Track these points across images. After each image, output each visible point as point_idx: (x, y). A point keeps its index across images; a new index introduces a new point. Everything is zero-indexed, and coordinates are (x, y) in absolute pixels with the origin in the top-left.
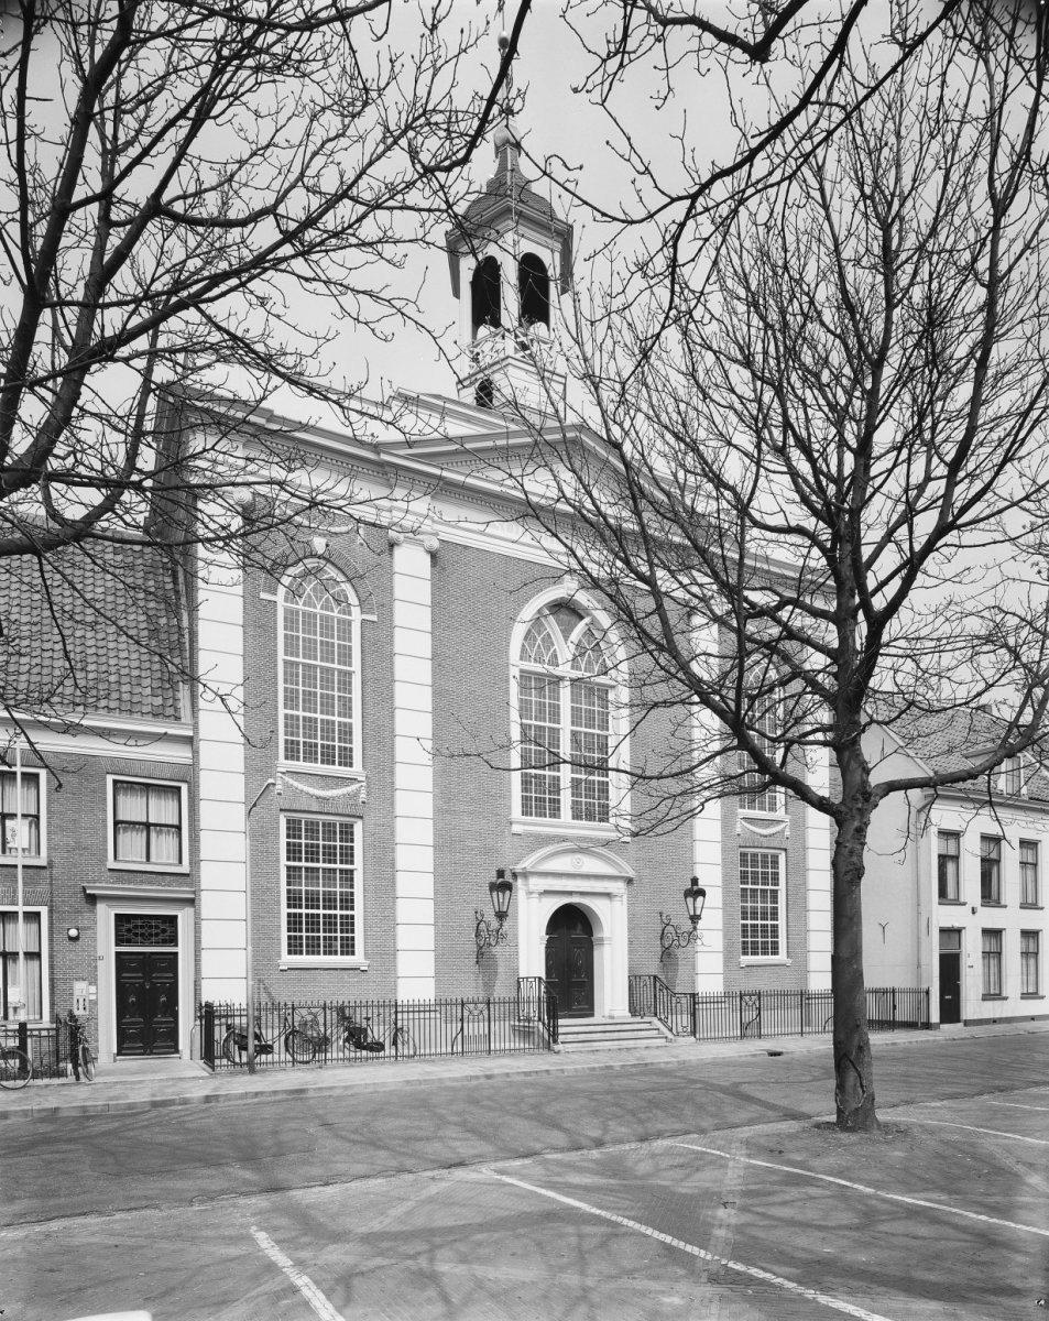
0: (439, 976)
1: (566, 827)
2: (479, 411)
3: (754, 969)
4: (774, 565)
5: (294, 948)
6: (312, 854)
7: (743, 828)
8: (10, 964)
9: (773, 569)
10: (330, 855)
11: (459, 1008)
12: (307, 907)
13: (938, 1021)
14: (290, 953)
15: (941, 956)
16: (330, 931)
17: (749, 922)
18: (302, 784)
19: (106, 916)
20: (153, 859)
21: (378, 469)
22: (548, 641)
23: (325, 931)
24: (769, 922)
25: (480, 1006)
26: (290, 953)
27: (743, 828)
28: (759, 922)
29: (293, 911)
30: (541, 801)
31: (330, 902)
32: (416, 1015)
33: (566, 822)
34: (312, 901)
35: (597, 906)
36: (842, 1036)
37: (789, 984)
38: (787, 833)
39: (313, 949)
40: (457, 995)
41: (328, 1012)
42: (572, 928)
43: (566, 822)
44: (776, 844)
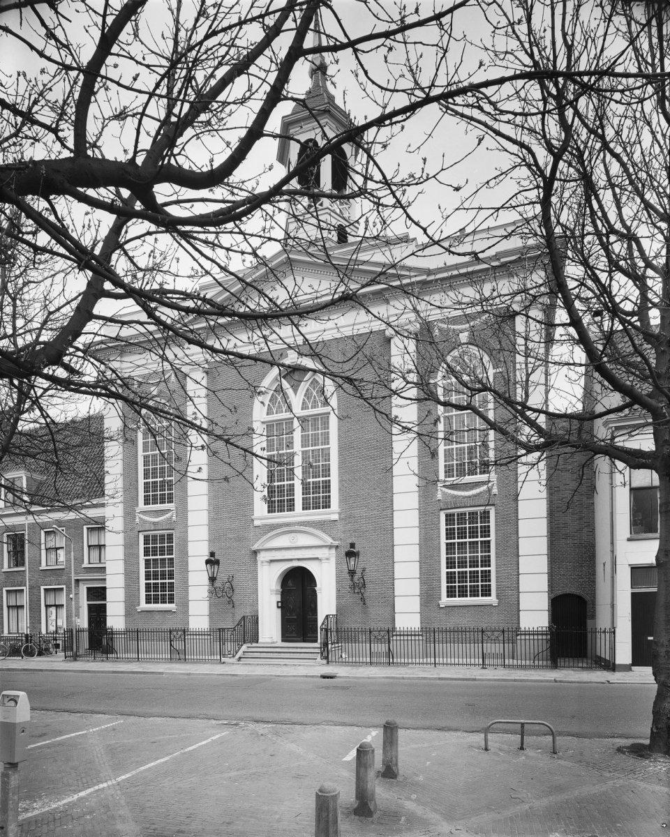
0: (211, 615)
1: (300, 516)
2: (341, 248)
3: (456, 609)
4: (463, 267)
5: (451, 593)
6: (462, 534)
7: (444, 493)
8: (20, 611)
9: (438, 276)
10: (473, 533)
11: (480, 634)
12: (470, 567)
13: (628, 661)
14: (448, 596)
15: (634, 596)
16: (463, 586)
17: (152, 581)
18: (150, 516)
19: (83, 590)
20: (102, 561)
21: (504, 269)
22: (285, 397)
23: (478, 582)
24: (152, 581)
25: (179, 633)
26: (448, 596)
27: (444, 493)
28: (167, 581)
29: (487, 569)
30: (279, 500)
31: (474, 563)
32: (413, 638)
33: (299, 513)
34: (462, 564)
35: (311, 567)
36: (662, 678)
37: (495, 621)
38: (495, 491)
39: (463, 593)
40: (134, 627)
41: (436, 634)
42: (298, 584)
43: (299, 513)
44: (482, 502)
